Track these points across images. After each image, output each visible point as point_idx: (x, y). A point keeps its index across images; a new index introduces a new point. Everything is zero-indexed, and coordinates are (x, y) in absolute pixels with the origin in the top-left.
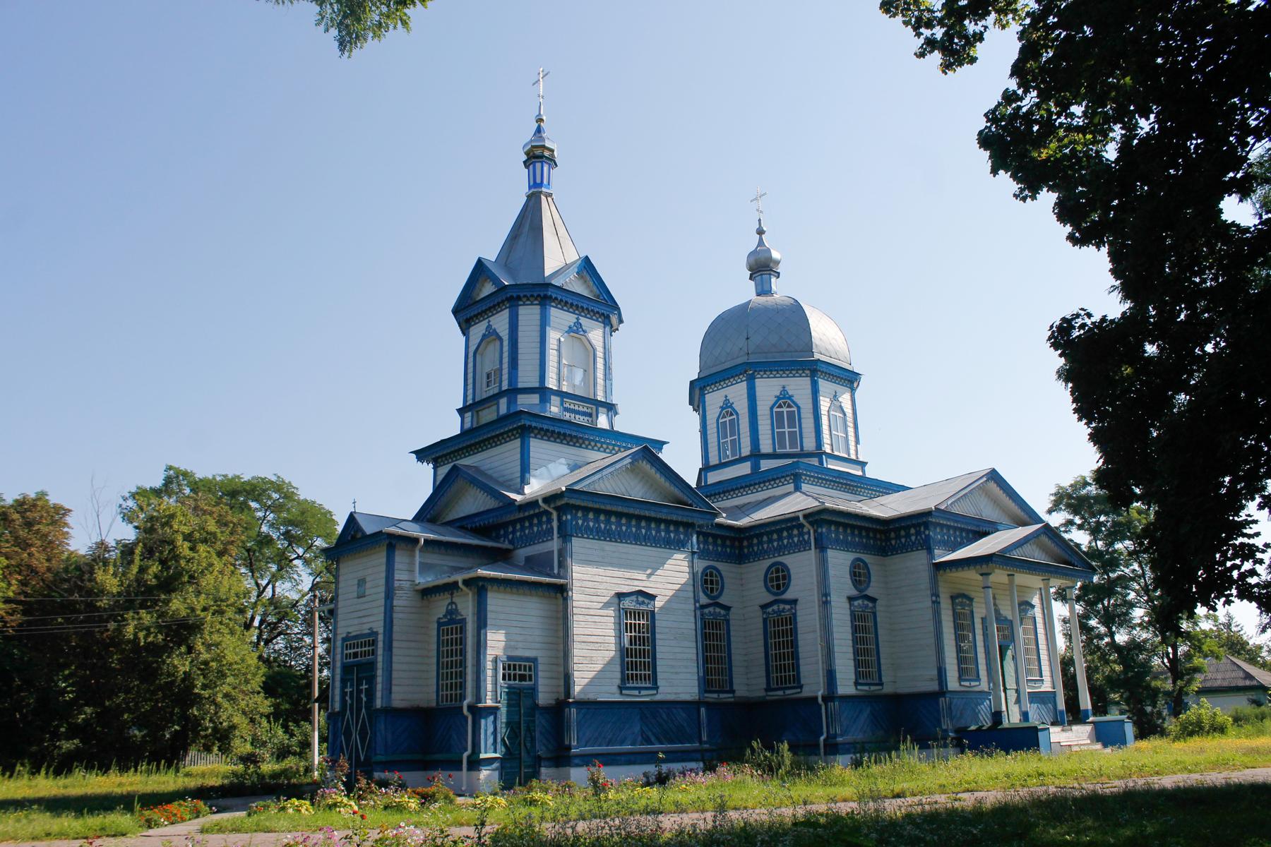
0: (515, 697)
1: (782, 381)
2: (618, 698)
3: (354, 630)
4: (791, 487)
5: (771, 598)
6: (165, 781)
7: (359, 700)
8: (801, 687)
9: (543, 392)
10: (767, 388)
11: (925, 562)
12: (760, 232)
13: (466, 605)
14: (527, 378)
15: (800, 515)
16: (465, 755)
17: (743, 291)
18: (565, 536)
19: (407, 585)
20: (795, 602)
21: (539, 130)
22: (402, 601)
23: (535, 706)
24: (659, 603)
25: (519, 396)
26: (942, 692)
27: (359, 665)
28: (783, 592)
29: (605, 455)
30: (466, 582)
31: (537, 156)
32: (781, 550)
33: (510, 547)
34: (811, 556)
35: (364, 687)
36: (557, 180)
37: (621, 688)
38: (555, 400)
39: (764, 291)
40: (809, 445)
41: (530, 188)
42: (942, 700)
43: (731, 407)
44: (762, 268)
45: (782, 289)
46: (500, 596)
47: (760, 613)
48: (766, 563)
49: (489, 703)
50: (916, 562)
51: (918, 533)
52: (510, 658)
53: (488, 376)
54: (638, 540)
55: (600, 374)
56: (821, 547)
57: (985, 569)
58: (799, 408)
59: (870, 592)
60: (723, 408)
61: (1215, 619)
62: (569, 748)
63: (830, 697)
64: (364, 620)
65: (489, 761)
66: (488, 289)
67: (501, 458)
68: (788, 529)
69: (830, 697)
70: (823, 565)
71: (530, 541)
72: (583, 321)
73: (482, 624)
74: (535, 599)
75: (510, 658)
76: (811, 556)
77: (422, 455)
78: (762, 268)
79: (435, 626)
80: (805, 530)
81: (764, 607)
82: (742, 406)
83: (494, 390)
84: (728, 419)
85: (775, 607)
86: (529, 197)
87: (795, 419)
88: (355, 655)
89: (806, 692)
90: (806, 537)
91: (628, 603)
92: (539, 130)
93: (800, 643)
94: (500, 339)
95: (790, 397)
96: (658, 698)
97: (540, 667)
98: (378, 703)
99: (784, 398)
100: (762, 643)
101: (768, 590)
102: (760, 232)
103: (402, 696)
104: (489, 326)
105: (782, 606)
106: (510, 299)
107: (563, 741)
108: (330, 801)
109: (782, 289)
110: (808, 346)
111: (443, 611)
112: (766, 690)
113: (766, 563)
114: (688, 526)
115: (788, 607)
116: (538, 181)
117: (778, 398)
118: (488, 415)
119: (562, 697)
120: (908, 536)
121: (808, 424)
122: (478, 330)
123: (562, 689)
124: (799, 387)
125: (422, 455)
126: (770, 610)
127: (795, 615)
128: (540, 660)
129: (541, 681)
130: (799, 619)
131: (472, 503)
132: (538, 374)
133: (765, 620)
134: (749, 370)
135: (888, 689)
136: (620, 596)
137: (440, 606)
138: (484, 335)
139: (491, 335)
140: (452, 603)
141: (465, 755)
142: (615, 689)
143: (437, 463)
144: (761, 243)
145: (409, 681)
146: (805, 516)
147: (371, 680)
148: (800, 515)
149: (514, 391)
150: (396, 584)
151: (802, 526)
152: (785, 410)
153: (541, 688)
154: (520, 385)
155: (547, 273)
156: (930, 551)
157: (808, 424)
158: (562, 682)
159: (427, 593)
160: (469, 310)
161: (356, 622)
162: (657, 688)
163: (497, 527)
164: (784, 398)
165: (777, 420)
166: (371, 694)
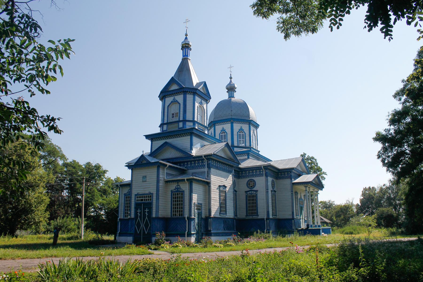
0: (199, 214)
1: (241, 125)
2: (219, 216)
3: (141, 191)
4: (246, 157)
5: (249, 189)
6: (13, 241)
7: (144, 215)
8: (258, 215)
9: (194, 122)
10: (237, 126)
11: (290, 182)
12: (231, 78)
13: (185, 187)
14: (189, 117)
15: (262, 166)
16: (186, 232)
17: (225, 96)
18: (209, 167)
19: (162, 179)
20: (257, 191)
21: (186, 38)
22: (161, 184)
23: (202, 218)
24: (227, 189)
25: (187, 123)
26: (293, 219)
27: (144, 204)
28: (253, 188)
29: (209, 144)
30: (187, 180)
31: (186, 47)
32: (253, 176)
33: (186, 169)
34: (264, 178)
35: (139, 211)
36: (192, 55)
37: (220, 213)
38: (197, 124)
39: (231, 96)
40: (248, 145)
41: (183, 56)
42: (293, 221)
43: (225, 130)
44: (231, 89)
45: (238, 97)
46: (197, 185)
47: (245, 194)
48: (248, 179)
49: (193, 217)
50: (287, 182)
51: (287, 174)
52: (198, 203)
53: (173, 114)
54: (224, 170)
55: (206, 118)
56: (267, 176)
57: (306, 185)
58: (245, 134)
59: (275, 189)
60: (221, 131)
61: (400, 205)
62: (210, 231)
63: (268, 219)
64: (145, 189)
65: (194, 234)
66: (174, 87)
67: (182, 142)
68: (198, 160)
69: (268, 219)
70: (267, 181)
71: (193, 168)
72: (202, 101)
73: (191, 192)
74: (201, 186)
75: (198, 203)
76: (264, 178)
77: (147, 137)
78: (231, 89)
79: (170, 192)
80: (204, 161)
81: (246, 192)
82: (228, 131)
83: (176, 119)
84: (223, 134)
85: (250, 192)
86: (183, 60)
87: (244, 137)
88: (142, 200)
89: (260, 217)
90: (262, 173)
91: (222, 189)
92: (186, 38)
93: (258, 203)
94: (179, 104)
95: (243, 130)
96: (227, 217)
97: (203, 206)
98: (154, 215)
99: (241, 130)
100: (245, 202)
101: (248, 187)
102: (231, 78)
103: (161, 214)
104: (174, 99)
105: (252, 192)
106: (183, 92)
107: (208, 228)
108: (175, 245)
109: (238, 97)
110: (248, 115)
111: (174, 188)
112: (246, 216)
113: (248, 179)
114: (232, 166)
115: (254, 192)
116: (187, 54)
117: (240, 130)
118: (174, 128)
119: (208, 215)
120: (285, 174)
121: (248, 138)
122: (169, 100)
123: (208, 213)
124: (245, 127)
125: (147, 137)
126: (248, 193)
127: (257, 195)
128: (203, 204)
129: (203, 211)
130: (258, 196)
131: (171, 154)
132: (192, 116)
133: (246, 196)
134: (232, 120)
135: (278, 217)
136: (220, 186)
137: (173, 187)
138: (172, 102)
139: (175, 102)
140: (178, 186)
141: (186, 232)
142: (219, 214)
143: (152, 140)
144: (231, 81)
145: (163, 208)
146: (264, 167)
147: (150, 208)
148: (262, 166)
149: (185, 121)
150: (160, 178)
151: (203, 159)
152: (241, 133)
153: (203, 213)
154: (187, 119)
155: (194, 85)
156: (291, 179)
157: (248, 138)
158: (208, 211)
159: (167, 182)
160: (164, 94)
161: (142, 189)
162: (226, 214)
163: (184, 162)
164: (241, 130)
165: (239, 136)
166: (150, 213)
